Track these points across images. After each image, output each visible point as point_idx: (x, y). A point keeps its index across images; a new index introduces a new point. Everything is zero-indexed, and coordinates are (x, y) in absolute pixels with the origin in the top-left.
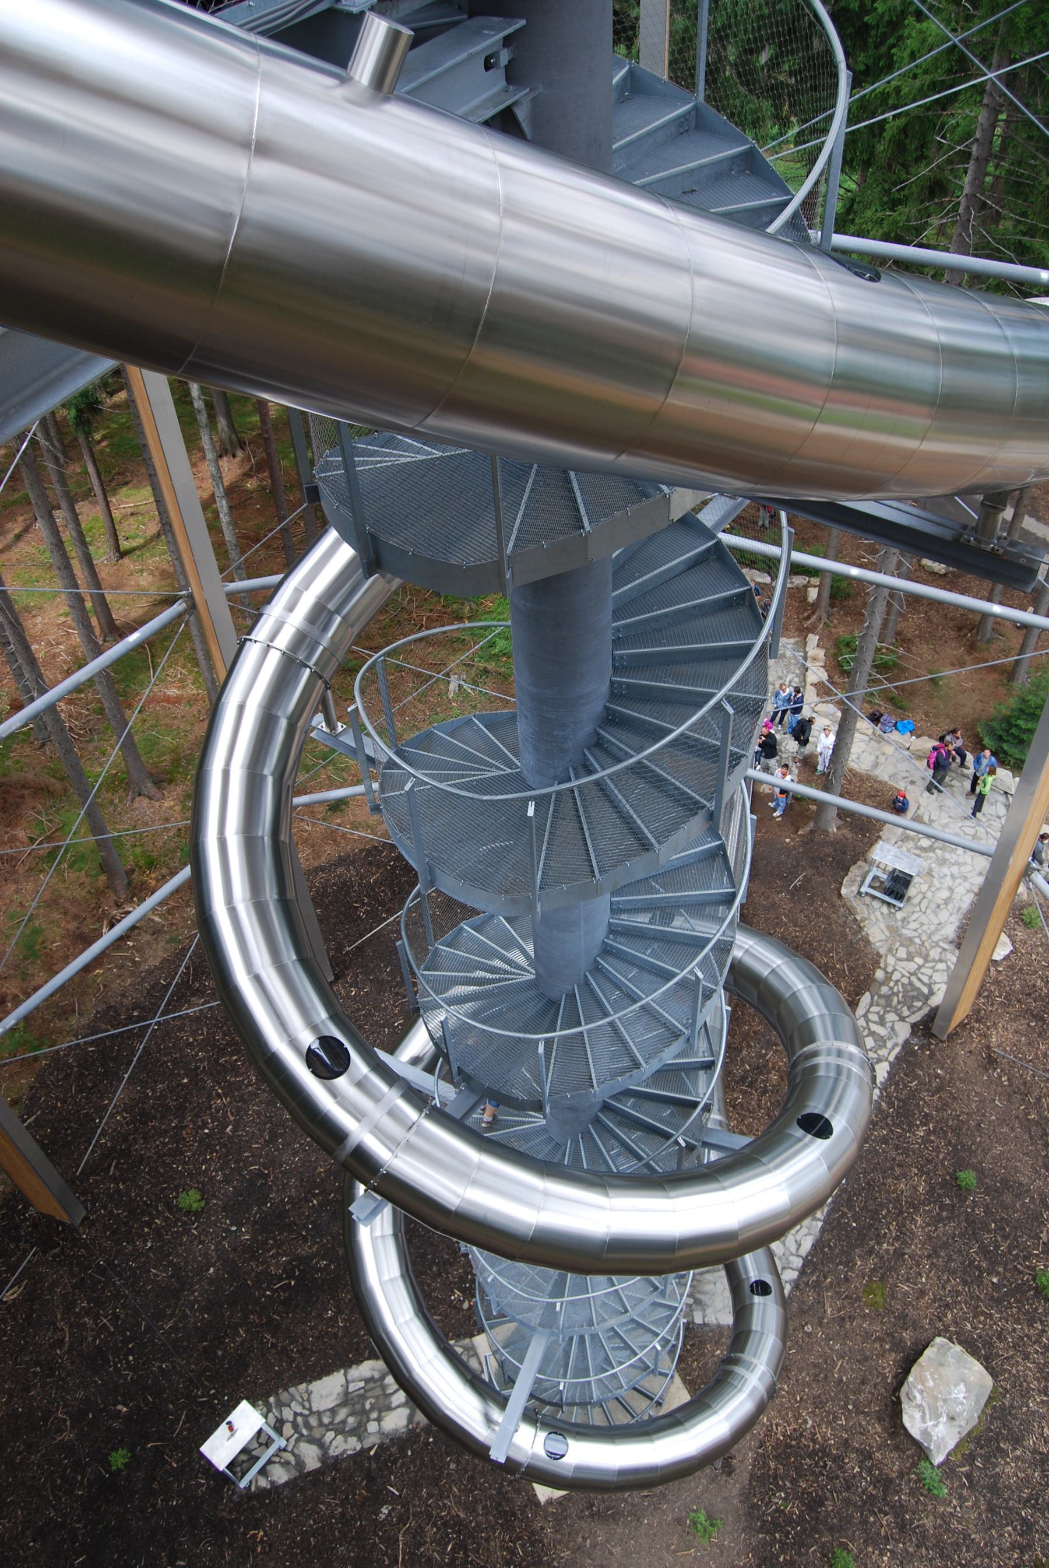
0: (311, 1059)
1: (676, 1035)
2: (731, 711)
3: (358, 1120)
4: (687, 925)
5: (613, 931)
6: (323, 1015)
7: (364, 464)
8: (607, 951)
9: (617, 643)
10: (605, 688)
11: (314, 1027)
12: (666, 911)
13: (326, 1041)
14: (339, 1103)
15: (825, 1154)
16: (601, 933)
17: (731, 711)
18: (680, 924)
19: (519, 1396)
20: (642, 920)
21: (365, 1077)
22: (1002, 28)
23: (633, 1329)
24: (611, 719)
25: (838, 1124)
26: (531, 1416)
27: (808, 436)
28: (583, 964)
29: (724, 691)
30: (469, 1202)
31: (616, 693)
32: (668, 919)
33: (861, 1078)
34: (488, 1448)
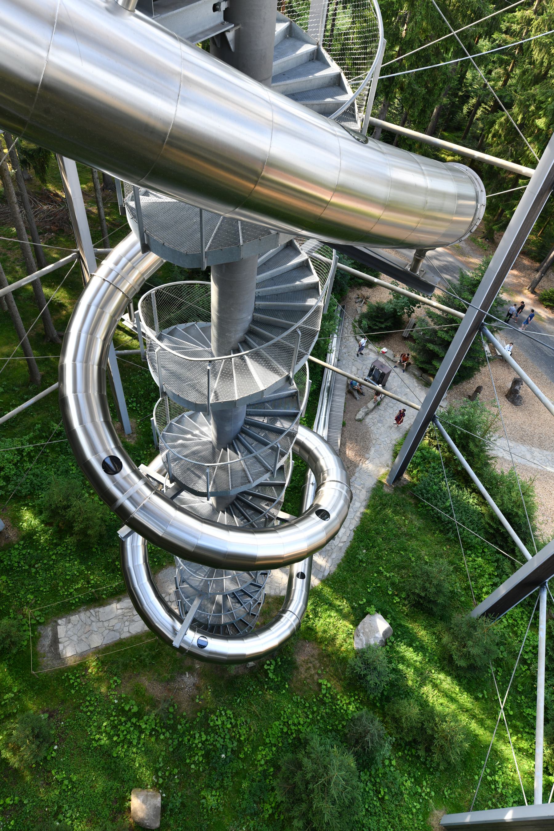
0: (105, 466)
1: (267, 470)
2: (300, 333)
3: (123, 493)
4: (529, 456)
5: (246, 423)
6: (113, 446)
7: (144, 200)
8: (242, 431)
9: (258, 298)
10: (250, 317)
11: (106, 451)
12: (274, 417)
13: (114, 459)
14: (115, 486)
15: (326, 527)
16: (240, 423)
17: (300, 333)
18: (278, 425)
19: (188, 619)
20: (264, 421)
21: (128, 475)
22: (459, 64)
23: (242, 595)
24: (250, 332)
25: (333, 515)
26: (192, 628)
27: (252, 191)
28: (232, 435)
29: (300, 323)
30: (170, 534)
31: (254, 321)
32: (275, 421)
33: (346, 497)
34: (172, 641)
